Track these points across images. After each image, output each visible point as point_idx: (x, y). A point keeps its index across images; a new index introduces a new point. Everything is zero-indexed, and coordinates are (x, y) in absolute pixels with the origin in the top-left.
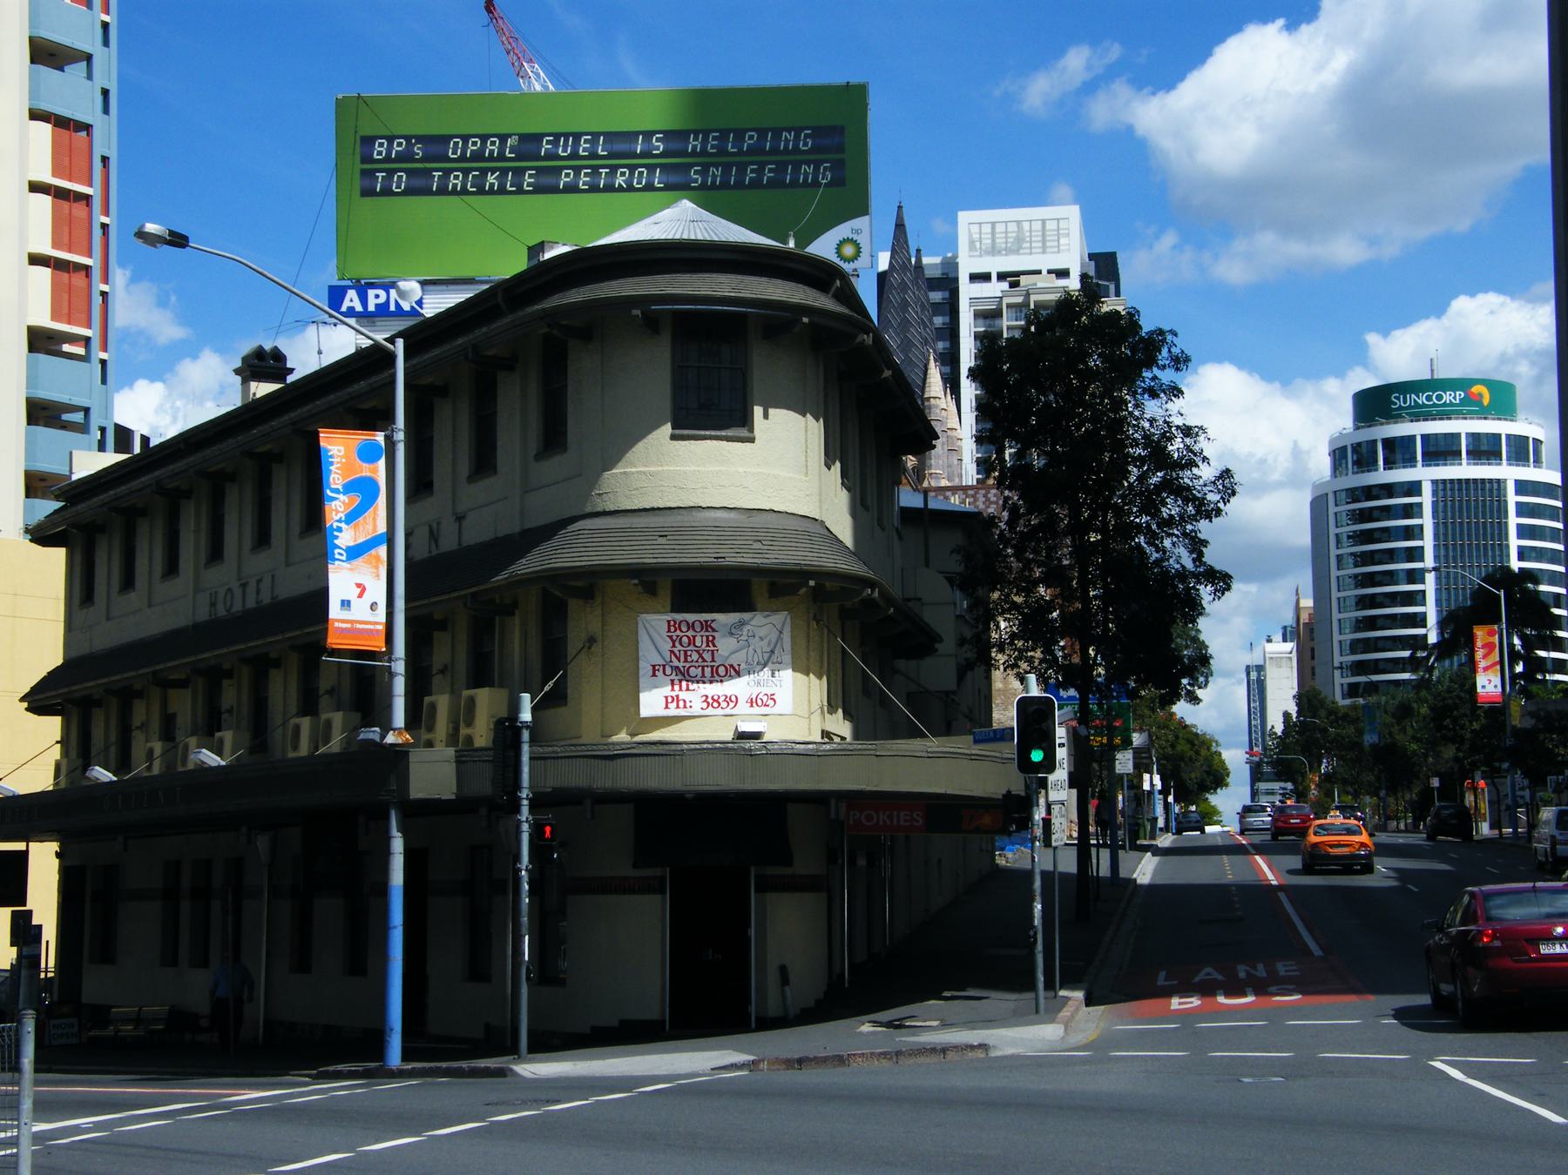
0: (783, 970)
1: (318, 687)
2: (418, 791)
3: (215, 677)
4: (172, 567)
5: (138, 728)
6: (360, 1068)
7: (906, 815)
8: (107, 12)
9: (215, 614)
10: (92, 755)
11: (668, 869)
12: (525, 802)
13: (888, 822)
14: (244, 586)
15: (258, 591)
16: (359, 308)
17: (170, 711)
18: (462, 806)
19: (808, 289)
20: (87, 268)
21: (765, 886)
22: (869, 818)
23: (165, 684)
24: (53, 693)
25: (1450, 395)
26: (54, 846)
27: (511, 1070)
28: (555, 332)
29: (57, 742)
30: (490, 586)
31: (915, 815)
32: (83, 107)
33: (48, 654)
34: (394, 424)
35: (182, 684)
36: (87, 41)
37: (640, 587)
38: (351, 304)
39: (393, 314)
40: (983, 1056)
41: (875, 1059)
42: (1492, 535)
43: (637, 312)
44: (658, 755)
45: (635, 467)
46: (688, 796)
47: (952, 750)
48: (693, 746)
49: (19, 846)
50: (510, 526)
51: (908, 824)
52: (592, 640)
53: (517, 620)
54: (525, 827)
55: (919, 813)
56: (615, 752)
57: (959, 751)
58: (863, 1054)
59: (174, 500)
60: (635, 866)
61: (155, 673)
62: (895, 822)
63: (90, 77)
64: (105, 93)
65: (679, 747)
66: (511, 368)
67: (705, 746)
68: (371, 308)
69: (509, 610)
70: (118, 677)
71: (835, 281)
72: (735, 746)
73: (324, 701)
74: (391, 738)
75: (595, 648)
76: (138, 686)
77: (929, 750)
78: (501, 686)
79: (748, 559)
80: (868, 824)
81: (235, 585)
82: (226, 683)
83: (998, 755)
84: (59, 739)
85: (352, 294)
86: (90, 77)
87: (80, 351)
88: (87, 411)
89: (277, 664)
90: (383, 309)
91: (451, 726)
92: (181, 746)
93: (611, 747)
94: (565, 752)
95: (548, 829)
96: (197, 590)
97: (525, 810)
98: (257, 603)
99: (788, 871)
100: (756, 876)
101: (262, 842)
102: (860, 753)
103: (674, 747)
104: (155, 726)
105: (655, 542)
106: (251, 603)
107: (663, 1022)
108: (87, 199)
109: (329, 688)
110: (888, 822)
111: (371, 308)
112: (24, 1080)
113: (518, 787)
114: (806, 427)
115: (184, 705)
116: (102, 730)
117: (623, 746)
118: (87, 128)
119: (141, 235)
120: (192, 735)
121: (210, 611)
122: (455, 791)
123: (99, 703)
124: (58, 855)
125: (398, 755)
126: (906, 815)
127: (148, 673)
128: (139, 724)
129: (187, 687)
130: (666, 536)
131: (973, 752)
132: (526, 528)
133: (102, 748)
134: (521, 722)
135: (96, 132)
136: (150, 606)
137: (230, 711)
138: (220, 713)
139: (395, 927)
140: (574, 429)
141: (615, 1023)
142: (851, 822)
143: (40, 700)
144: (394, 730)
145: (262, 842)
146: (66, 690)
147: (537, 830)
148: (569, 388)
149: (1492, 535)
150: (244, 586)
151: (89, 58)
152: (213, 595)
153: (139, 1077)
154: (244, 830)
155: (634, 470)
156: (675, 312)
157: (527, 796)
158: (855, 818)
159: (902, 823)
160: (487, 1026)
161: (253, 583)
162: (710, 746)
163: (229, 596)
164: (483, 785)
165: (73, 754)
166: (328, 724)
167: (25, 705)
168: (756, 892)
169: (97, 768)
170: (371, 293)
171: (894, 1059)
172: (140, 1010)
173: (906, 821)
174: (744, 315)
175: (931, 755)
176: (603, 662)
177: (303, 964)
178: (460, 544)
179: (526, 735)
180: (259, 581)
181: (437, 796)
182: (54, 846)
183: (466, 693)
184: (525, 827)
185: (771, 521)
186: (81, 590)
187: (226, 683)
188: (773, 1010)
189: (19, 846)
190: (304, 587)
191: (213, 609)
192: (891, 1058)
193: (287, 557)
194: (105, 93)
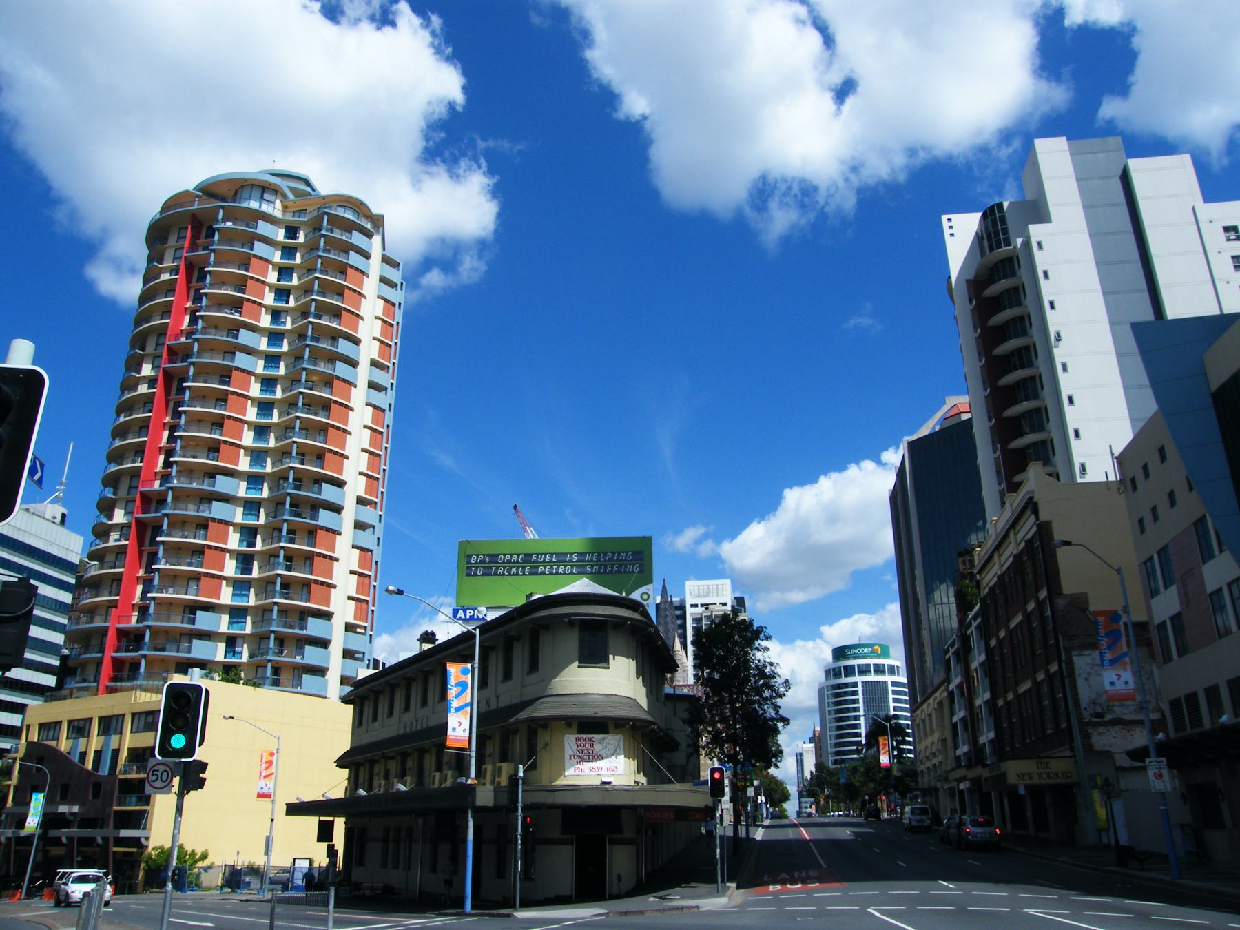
0: (619, 876)
3: (404, 756)
4: (391, 714)
12: (520, 808)
14: (417, 721)
15: (422, 723)
16: (463, 617)
21: (613, 842)
23: (387, 758)
26: (343, 819)
33: (345, 746)
35: (393, 758)
43: (566, 619)
50: (517, 700)
52: (547, 745)
53: (518, 736)
54: (520, 818)
63: (374, 533)
64: (378, 539)
68: (468, 617)
69: (516, 732)
73: (445, 767)
74: (469, 782)
75: (548, 748)
78: (512, 762)
85: (461, 612)
86: (374, 533)
88: (364, 653)
89: (428, 751)
90: (472, 617)
95: (528, 819)
96: (400, 722)
97: (520, 811)
101: (420, 821)
104: (382, 773)
106: (419, 728)
107: (572, 896)
111: (468, 617)
115: (393, 766)
118: (372, 551)
119: (387, 590)
120: (396, 777)
123: (362, 765)
125: (472, 788)
137: (410, 769)
140: (541, 666)
143: (341, 762)
150: (417, 721)
151: (374, 527)
160: (504, 897)
165: (352, 783)
166: (446, 775)
167: (336, 764)
170: (468, 611)
179: (521, 781)
182: (343, 819)
184: (520, 818)
186: (358, 721)
188: (615, 891)
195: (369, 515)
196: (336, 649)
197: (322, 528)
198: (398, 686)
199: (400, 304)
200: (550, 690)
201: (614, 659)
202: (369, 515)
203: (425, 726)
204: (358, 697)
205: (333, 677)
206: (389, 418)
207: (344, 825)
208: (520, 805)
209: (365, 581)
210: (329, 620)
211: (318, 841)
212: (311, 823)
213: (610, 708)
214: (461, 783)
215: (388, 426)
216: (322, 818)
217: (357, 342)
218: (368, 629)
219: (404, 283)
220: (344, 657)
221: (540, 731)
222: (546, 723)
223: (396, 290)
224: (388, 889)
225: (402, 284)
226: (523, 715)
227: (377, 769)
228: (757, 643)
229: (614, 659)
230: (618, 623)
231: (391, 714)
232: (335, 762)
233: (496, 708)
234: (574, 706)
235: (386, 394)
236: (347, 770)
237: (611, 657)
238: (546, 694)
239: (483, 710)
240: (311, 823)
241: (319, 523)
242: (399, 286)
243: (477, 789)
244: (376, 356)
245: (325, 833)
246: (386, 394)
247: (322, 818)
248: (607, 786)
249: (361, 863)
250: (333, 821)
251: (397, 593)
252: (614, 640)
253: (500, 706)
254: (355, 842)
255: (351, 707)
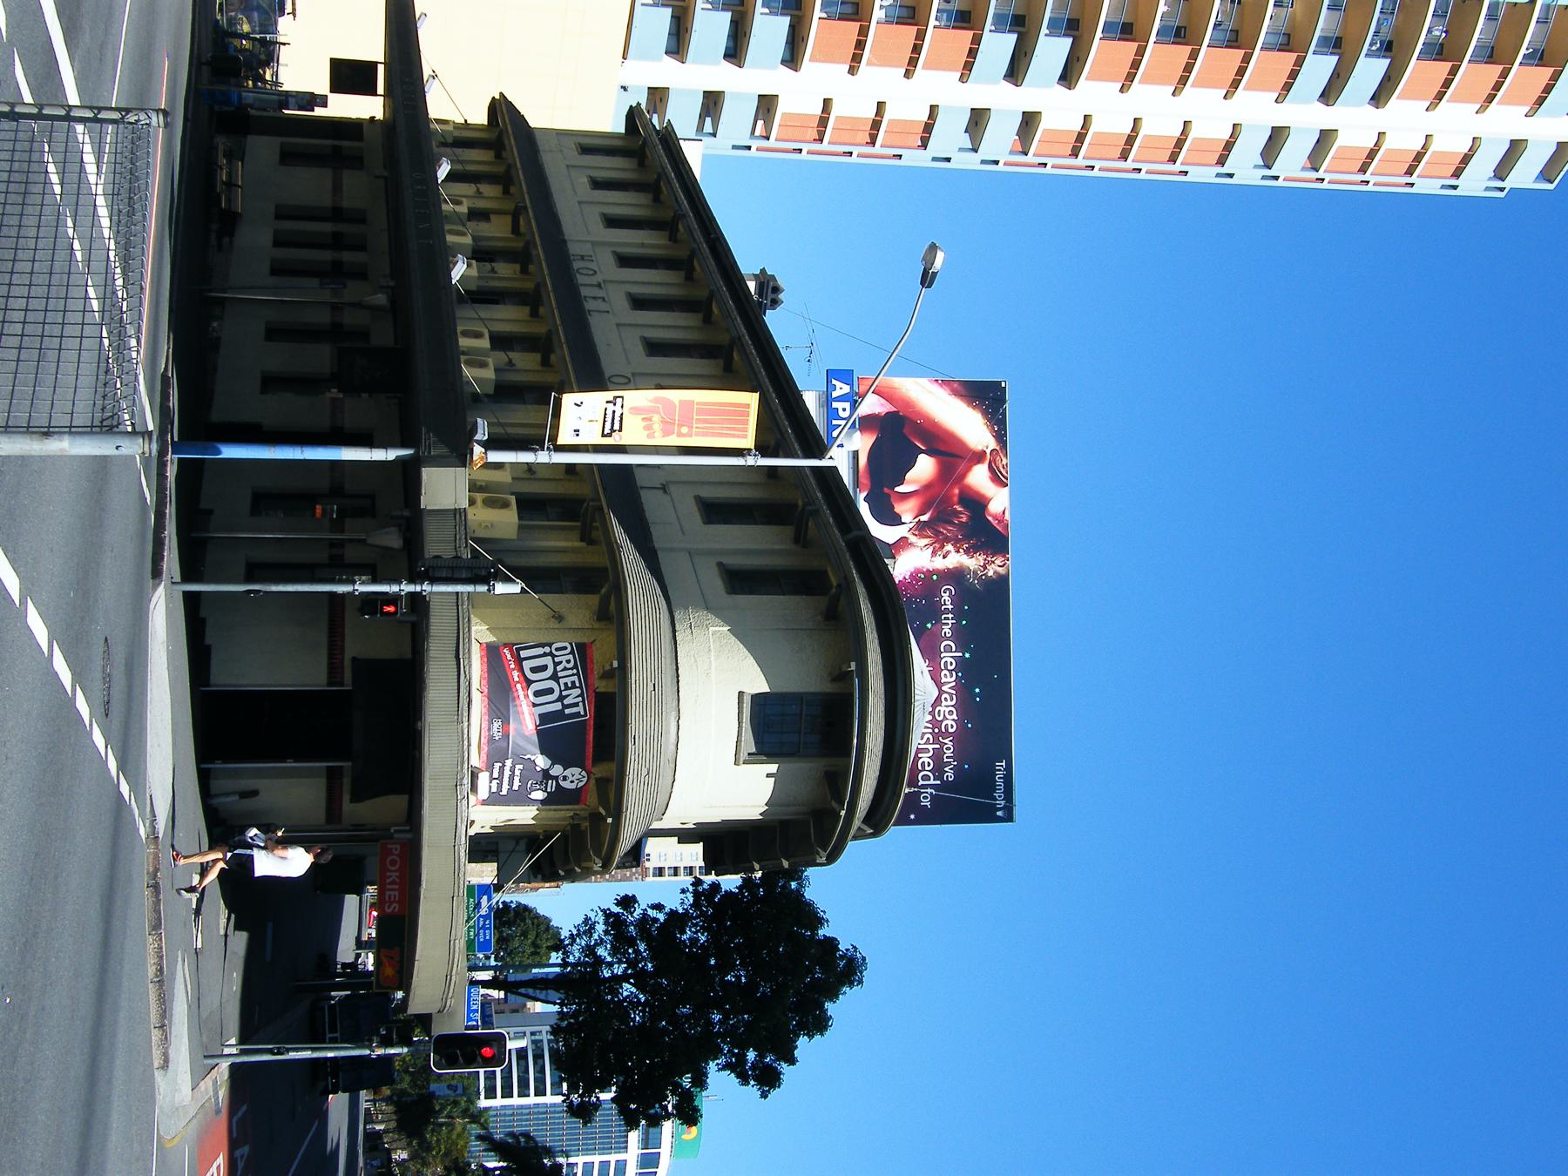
0: (255, 793)
1: (513, 351)
2: (429, 475)
3: (522, 258)
4: (612, 222)
5: (478, 190)
6: (171, 405)
7: (395, 898)
8: (1005, 164)
9: (574, 260)
10: (454, 149)
11: (350, 688)
12: (418, 588)
13: (388, 881)
14: (599, 286)
15: (594, 298)
16: (835, 394)
17: (492, 216)
18: (412, 519)
19: (865, 813)
20: (821, 140)
21: (333, 776)
22: (393, 863)
23: (516, 215)
24: (507, 121)
25: (568, 661)
26: (379, 116)
27: (159, 584)
28: (834, 590)
29: (466, 121)
30: (606, 511)
31: (395, 905)
32: (937, 145)
33: (537, 118)
34: (762, 456)
35: (515, 229)
36: (986, 151)
37: (609, 668)
38: (838, 388)
39: (829, 422)
40: (156, 1065)
41: (156, 961)
42: (587, 1144)
43: (853, 666)
44: (459, 692)
45: (715, 660)
46: (419, 724)
47: (456, 960)
48: (466, 732)
49: (381, 89)
50: (659, 542)
51: (387, 899)
52: (559, 618)
53: (578, 544)
54: (395, 588)
55: (397, 910)
56: (462, 660)
57: (455, 966)
58: (161, 948)
59: (668, 226)
60: (354, 659)
61: (525, 208)
62: (389, 887)
63: (961, 150)
64: (948, 160)
65: (465, 719)
66: (797, 540)
67: (466, 743)
68: (835, 405)
69: (586, 537)
70: (522, 177)
71: (871, 828)
72: (465, 771)
73: (501, 357)
74: (478, 450)
75: (554, 624)
76: (513, 190)
77: (457, 941)
78: (521, 527)
79: (632, 767)
80: (388, 863)
81: (599, 278)
82: (517, 267)
83: (450, 994)
84: (468, 122)
85: (846, 389)
86: (961, 150)
87: (758, 133)
88: (714, 135)
89: (534, 314)
90: (832, 414)
91: (483, 484)
92: (461, 228)
93: (467, 656)
94: (463, 611)
95: (391, 609)
96: (594, 244)
97: (411, 588)
98: (585, 297)
99: (346, 798)
100: (342, 767)
101: (381, 299)
102: (456, 885)
103: (466, 714)
104: (481, 204)
105: (649, 680)
106: (584, 291)
107: (208, 686)
108: (873, 143)
109: (513, 361)
110: (388, 881)
111: (835, 405)
112: (28, 441)
113: (433, 581)
114: (746, 806)
115: (497, 230)
116: (478, 158)
117: (467, 668)
118: (924, 145)
119: (933, 248)
120: (474, 238)
121: (577, 255)
122: (428, 508)
123: (498, 156)
124: (372, 118)
125: (461, 457)
126: (395, 898)
127: (524, 202)
128: (481, 190)
129: (513, 233)
130: (654, 690)
131: (453, 978)
132: (660, 555)
133: (460, 158)
134: (494, 584)
135: (921, 152)
136: (579, 203)
137: (493, 270)
138: (491, 261)
139: (302, 451)
140: (743, 600)
141: (208, 641)
142: (390, 846)
143: (501, 109)
144: (485, 453)
145: (381, 299)
146: (510, 132)
147: (393, 599)
148: (782, 597)
149: (587, 1144)
150: (599, 286)
151: (975, 150)
152: (590, 258)
153: (176, 187)
154: (392, 284)
155: (713, 658)
156: (851, 695)
157: (425, 591)
158: (394, 851)
159: (388, 893)
160: (210, 512)
161: (600, 293)
162: (465, 747)
163: (591, 272)
164: (437, 544)
165: (457, 134)
166: (483, 365)
167: (497, 97)
168: (328, 767)
169: (449, 167)
170: (847, 405)
171: (155, 980)
172: (239, 186)
173: (390, 896)
174: (849, 755)
175: (452, 942)
176: (540, 629)
177: (274, 333)
178: (642, 488)
179: (482, 588)
180: (603, 299)
181: (423, 492)
182: (379, 116)
183: (513, 499)
184: (395, 588)
185: (665, 782)
186: (590, 145)
187: (517, 267)
188: (217, 785)
189: (381, 89)
190: (610, 363)
191: (579, 257)
192: (157, 976)
193: (624, 325)
194: (948, 160)
195: (1000, 137)
196: (723, 76)
197: (977, 40)
198: (673, 238)
199: (1455, 187)
200: (686, 624)
201: (768, 775)
202: (1000, 137)
203: (589, 305)
204: (645, 143)
205: (666, 72)
206: (1204, 174)
207: (368, 117)
208: (426, 587)
209: (861, 133)
210: (783, 62)
211: (331, 59)
212: (370, 46)
213: (645, 772)
214: (474, 430)
215: (1186, 173)
216: (381, 69)
217: (1379, 97)
218: (764, 143)
219: (1502, 195)
220: (707, 94)
221: (594, 600)
222: (613, 616)
223: (1490, 179)
224: (230, 221)
225: (1502, 189)
226: (631, 561)
227: (488, 190)
228: (474, 262)
229: (768, 775)
230: (837, 783)
231: (612, 222)
232: (501, 93)
233: (639, 484)
234: (651, 688)
235: (1256, 167)
236: (486, 123)
237: (773, 768)
238: (677, 616)
239: (641, 479)
240: (370, 46)
241: (987, 36)
242: (1500, 184)
243: (460, 470)
244: (1341, 141)
245: (350, 76)
246: (1256, 167)
247: (381, 69)
248: (467, 781)
249: (289, 157)
250: (374, 93)
251: (925, 273)
252: (807, 769)
253: (645, 495)
254: (329, 142)
255: (620, 128)
